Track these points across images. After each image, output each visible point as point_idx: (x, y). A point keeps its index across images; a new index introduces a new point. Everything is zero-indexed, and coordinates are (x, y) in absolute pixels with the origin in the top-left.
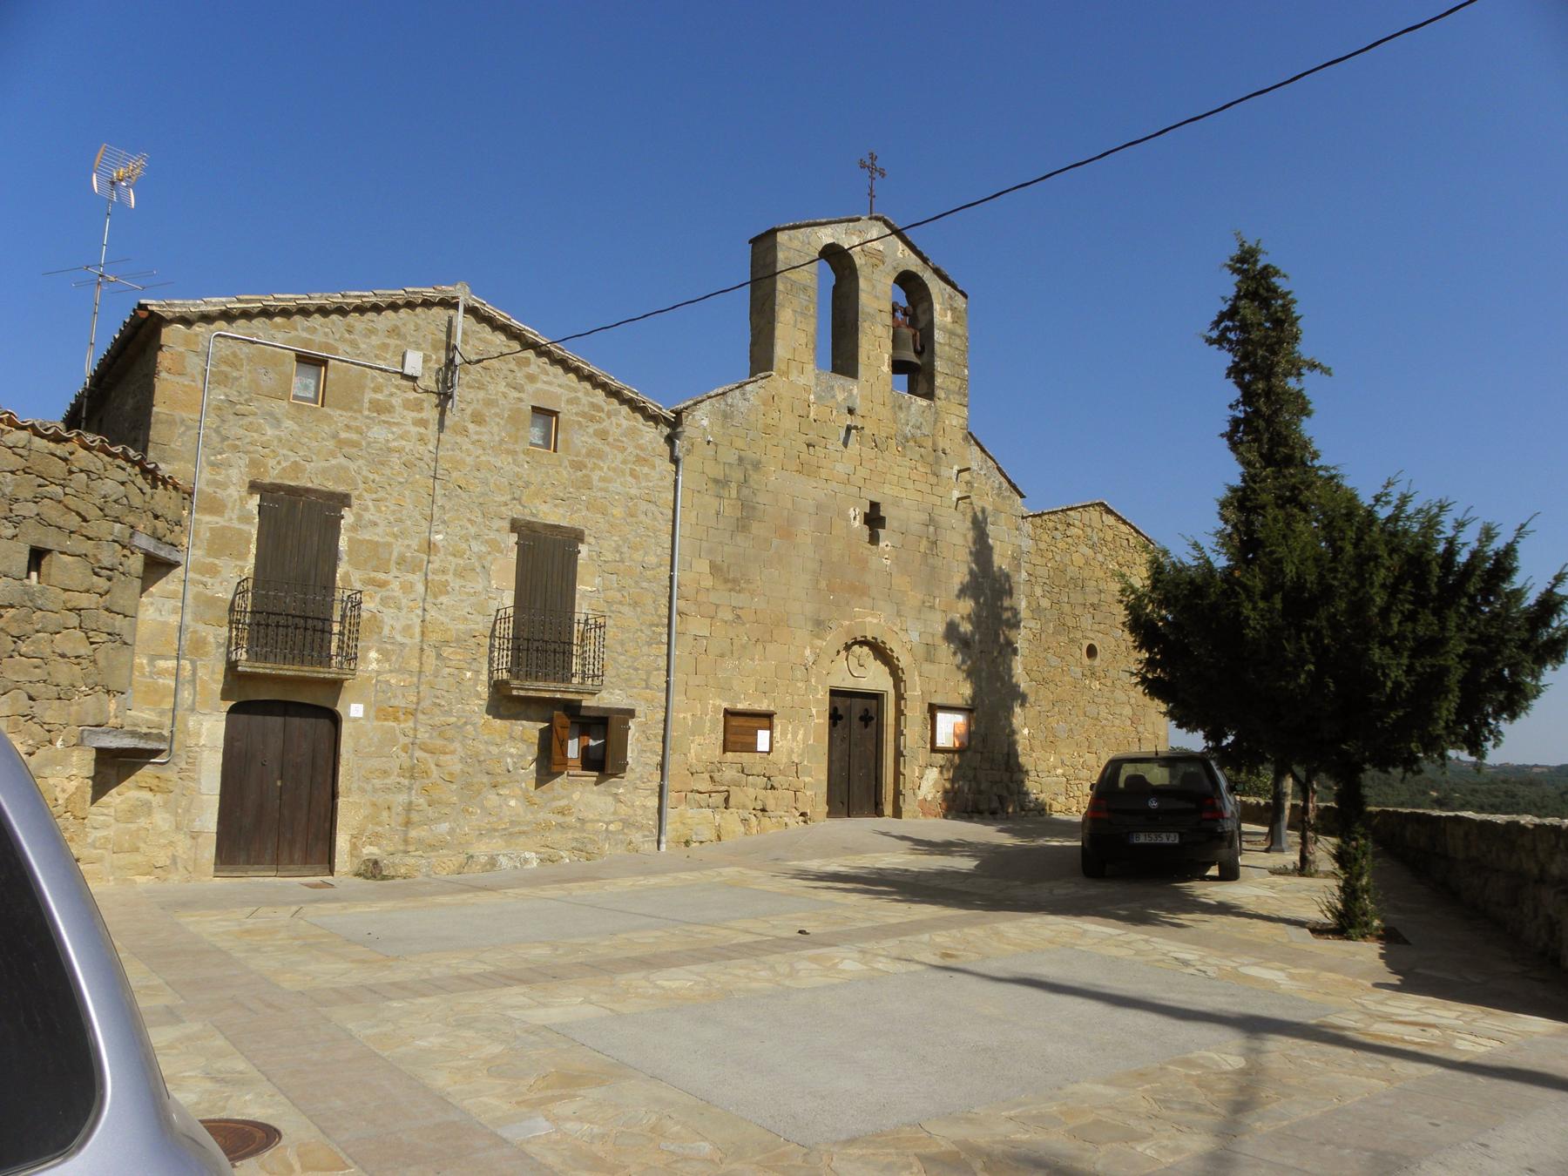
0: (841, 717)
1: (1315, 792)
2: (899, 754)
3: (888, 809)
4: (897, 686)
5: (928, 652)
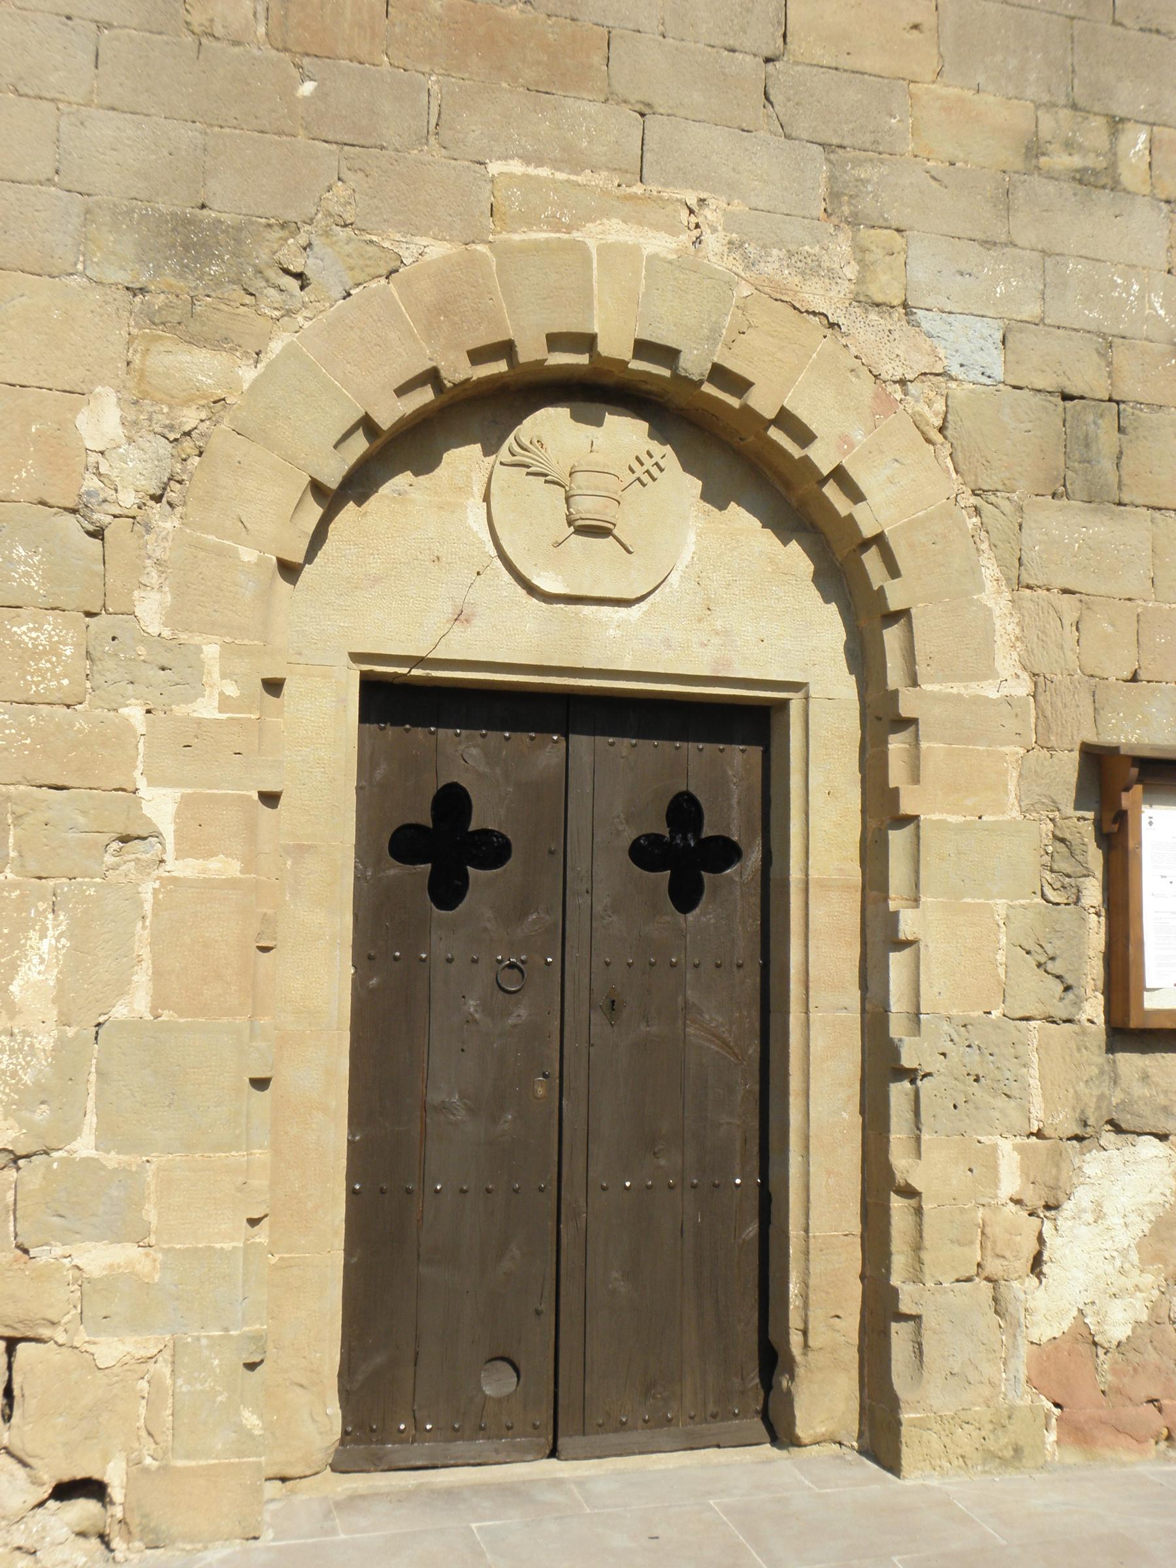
0: (493, 850)
1: (936, 415)
2: (882, 1066)
3: (825, 1395)
4: (863, 657)
5: (1078, 447)
